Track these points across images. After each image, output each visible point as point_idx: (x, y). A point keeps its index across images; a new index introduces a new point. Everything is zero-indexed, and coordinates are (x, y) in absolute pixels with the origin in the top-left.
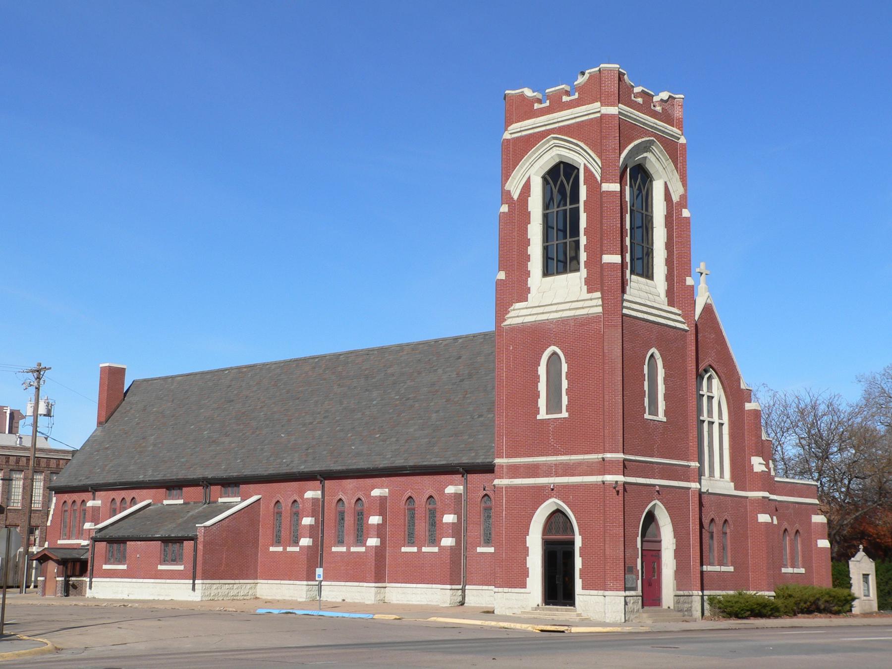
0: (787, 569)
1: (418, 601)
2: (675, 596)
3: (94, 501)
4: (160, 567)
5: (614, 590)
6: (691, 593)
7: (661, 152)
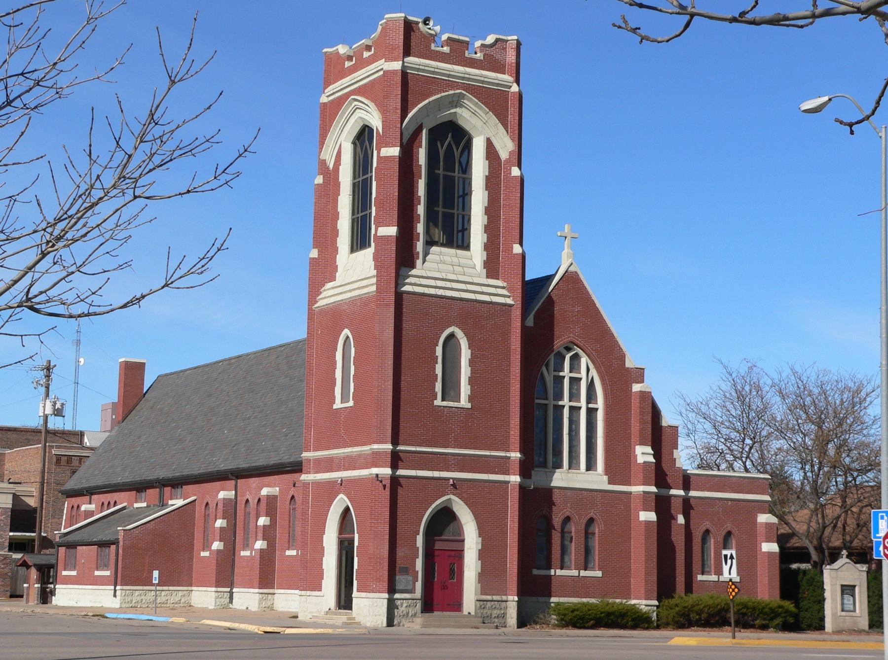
0: (710, 576)
1: (295, 608)
2: (478, 600)
3: (90, 505)
4: (97, 573)
5: (376, 592)
6: (504, 598)
7: (476, 105)
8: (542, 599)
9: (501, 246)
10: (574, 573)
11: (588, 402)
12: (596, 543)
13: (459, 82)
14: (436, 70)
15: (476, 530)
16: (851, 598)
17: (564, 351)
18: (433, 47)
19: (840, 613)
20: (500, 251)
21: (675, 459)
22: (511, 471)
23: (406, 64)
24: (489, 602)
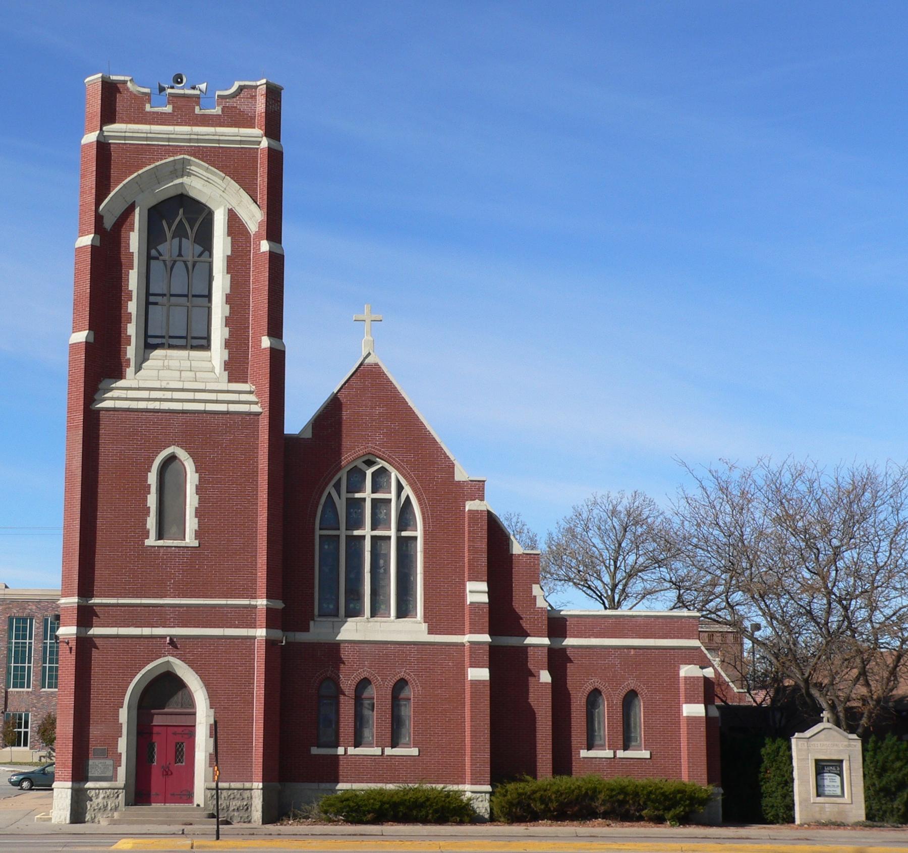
6: (248, 785)
7: (207, 170)
8: (328, 786)
9: (250, 341)
10: (608, 753)
11: (400, 528)
12: (408, 712)
13: (184, 146)
14: (149, 135)
15: (205, 699)
16: (838, 778)
17: (363, 467)
18: (148, 108)
19: (813, 798)
20: (249, 347)
21: (535, 597)
22: (258, 623)
23: (106, 134)
24: (225, 791)
